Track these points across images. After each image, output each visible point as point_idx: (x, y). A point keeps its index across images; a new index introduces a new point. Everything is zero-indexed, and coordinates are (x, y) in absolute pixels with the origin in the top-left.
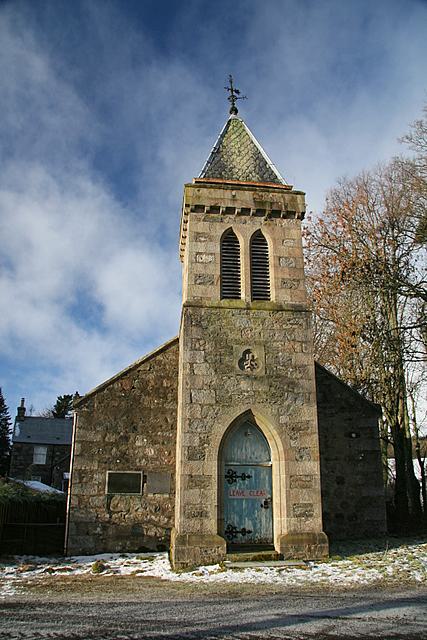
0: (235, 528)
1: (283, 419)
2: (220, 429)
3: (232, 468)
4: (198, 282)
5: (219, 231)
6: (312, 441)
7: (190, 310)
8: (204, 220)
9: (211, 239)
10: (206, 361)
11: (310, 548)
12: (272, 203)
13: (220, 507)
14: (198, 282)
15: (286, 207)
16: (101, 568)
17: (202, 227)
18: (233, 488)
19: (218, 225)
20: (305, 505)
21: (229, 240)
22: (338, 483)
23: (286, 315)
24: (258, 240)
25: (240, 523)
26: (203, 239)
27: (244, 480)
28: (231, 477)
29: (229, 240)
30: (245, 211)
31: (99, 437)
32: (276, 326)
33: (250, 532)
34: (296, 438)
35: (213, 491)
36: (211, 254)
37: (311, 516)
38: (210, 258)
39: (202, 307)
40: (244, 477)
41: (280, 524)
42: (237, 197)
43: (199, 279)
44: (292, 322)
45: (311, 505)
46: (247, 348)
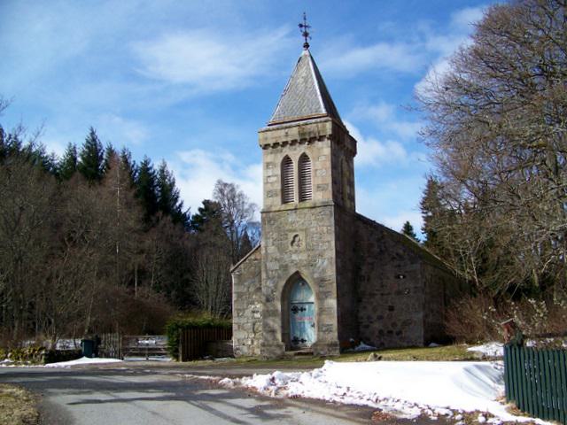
2: (283, 283)
5: (279, 158)
7: (264, 215)
8: (271, 153)
10: (273, 245)
12: (310, 133)
16: (556, 342)
17: (270, 158)
21: (287, 161)
23: (319, 210)
25: (301, 335)
30: (294, 142)
31: (246, 289)
32: (313, 218)
38: (274, 179)
41: (311, 336)
46: (295, 234)
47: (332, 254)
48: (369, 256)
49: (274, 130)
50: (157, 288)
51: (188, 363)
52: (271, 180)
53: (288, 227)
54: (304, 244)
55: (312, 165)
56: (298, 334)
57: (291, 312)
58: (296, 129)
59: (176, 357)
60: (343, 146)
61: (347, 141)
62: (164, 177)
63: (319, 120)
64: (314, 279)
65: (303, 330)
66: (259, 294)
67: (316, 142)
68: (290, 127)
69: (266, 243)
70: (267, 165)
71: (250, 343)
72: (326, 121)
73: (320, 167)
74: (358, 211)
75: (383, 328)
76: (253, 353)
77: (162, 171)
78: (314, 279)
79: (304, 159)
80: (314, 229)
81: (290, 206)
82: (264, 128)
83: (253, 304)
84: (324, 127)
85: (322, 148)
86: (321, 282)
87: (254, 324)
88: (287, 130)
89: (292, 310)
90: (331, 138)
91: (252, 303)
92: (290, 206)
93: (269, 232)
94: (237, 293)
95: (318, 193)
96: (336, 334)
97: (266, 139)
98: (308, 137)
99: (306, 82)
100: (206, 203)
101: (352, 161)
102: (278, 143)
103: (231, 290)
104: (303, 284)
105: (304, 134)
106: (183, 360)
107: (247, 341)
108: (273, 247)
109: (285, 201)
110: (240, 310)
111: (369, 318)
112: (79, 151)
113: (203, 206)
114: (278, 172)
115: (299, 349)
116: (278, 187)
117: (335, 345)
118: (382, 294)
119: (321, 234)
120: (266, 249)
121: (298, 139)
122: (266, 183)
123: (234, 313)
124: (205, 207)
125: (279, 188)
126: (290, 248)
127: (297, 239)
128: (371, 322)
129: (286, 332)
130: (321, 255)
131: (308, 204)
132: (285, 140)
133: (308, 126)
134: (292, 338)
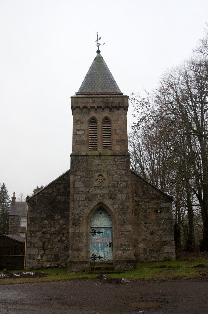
0: (96, 256)
3: (94, 229)
4: (77, 144)
7: (73, 157)
9: (82, 123)
11: (127, 264)
14: (77, 144)
19: (86, 116)
21: (93, 121)
22: (151, 234)
24: (107, 120)
25: (98, 253)
27: (99, 234)
28: (94, 233)
29: (93, 121)
33: (102, 257)
36: (84, 130)
38: (83, 132)
40: (99, 233)
48: (136, 196)
67: (115, 110)
68: (97, 97)
74: (70, 168)
75: (146, 248)
78: (115, 209)
97: (77, 102)
98: (110, 105)
110: (32, 231)
118: (145, 223)
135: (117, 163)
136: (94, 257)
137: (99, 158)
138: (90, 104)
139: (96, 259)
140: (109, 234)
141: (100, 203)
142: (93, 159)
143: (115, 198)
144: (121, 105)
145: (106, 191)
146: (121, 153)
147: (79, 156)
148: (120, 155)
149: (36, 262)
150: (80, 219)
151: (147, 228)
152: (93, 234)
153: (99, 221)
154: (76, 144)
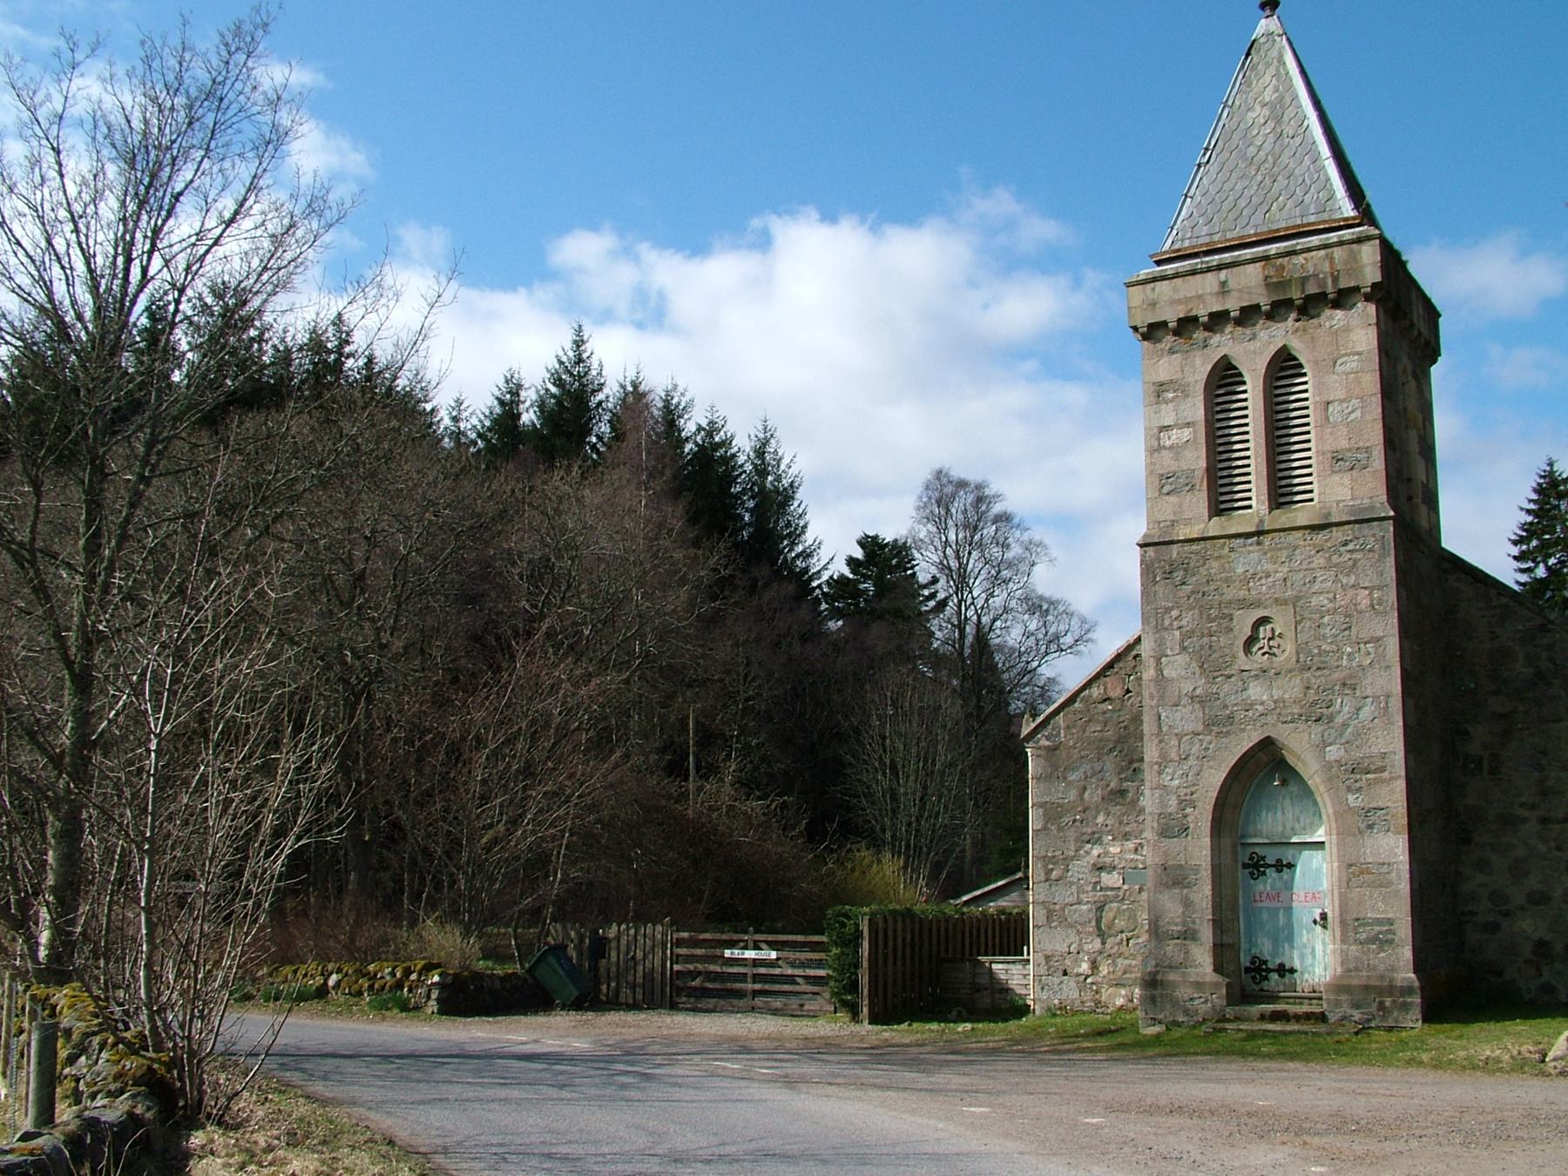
0: (1265, 962)
1: (1333, 752)
2: (1215, 777)
3: (1257, 850)
4: (1165, 490)
5: (1199, 368)
6: (1394, 795)
7: (1151, 551)
8: (1171, 352)
9: (1184, 391)
10: (1184, 649)
12: (1303, 281)
13: (1219, 924)
14: (1165, 490)
15: (1335, 280)
17: (1166, 367)
18: (1261, 887)
20: (1379, 922)
21: (1225, 377)
23: (1338, 534)
25: (1275, 954)
26: (1171, 395)
30: (1248, 315)
31: (1073, 795)
32: (1320, 560)
34: (1359, 790)
35: (1203, 893)
36: (1188, 425)
37: (1390, 942)
38: (1186, 434)
39: (1172, 542)
41: (1317, 959)
42: (1231, 284)
43: (1165, 483)
44: (1350, 547)
45: (1390, 922)
47: (1390, 681)
49: (1177, 275)
50: (748, 785)
51: (887, 1033)
52: (1175, 437)
53: (1231, 593)
54: (1287, 651)
55: (1310, 388)
56: (1265, 948)
57: (1242, 874)
58: (1254, 273)
59: (855, 1017)
60: (1408, 326)
61: (1418, 311)
62: (762, 471)
63: (1333, 237)
64: (1328, 766)
65: (1285, 935)
66: (1117, 810)
69: (1160, 643)
70: (1159, 391)
71: (1085, 967)
72: (1359, 240)
73: (1341, 394)
74: (1449, 542)
75: (1548, 937)
76: (1098, 1003)
77: (760, 452)
78: (1328, 766)
79: (1284, 367)
80: (1323, 599)
81: (1240, 522)
82: (1144, 273)
83: (1099, 841)
84: (1354, 257)
85: (1347, 329)
86: (1357, 771)
87: (1100, 909)
88: (1223, 275)
89: (1247, 863)
90: (1377, 294)
91: (1095, 839)
92: (1240, 522)
93: (1168, 610)
94: (1042, 805)
95: (1336, 478)
96: (1407, 953)
98: (1296, 295)
99: (1279, 121)
100: (871, 544)
101: (1427, 376)
102: (1195, 319)
103: (1216, 849)
104: (1284, 782)
105: (1283, 285)
106: (874, 1020)
107: (1077, 962)
108: (1182, 659)
109: (1220, 505)
111: (1498, 897)
112: (529, 396)
113: (859, 554)
114: (1196, 409)
115: (1273, 998)
116: (1197, 460)
117: (1408, 990)
118: (1544, 821)
119: (1349, 616)
120: (1158, 661)
121: (1264, 302)
122: (1154, 450)
123: (1034, 869)
124: (867, 555)
125: (1203, 464)
126: (1242, 661)
127: (1264, 632)
128: (1507, 914)
129: (1227, 939)
130: (1349, 685)
131: (1301, 515)
132: (1216, 307)
133: (1300, 259)
134: (1245, 960)
135: (1335, 559)
136: (1258, 970)
137: (1259, 544)
138: (1209, 299)
139: (1266, 978)
140: (1319, 870)
141: (1267, 744)
142: (1232, 550)
143: (1331, 718)
144: (1343, 284)
145: (1290, 689)
146: (1352, 513)
147: (1172, 542)
148: (1349, 523)
149: (1072, 984)
150: (1189, 810)
151: (1553, 845)
152: (1252, 874)
153: (1279, 814)
154: (1161, 494)
